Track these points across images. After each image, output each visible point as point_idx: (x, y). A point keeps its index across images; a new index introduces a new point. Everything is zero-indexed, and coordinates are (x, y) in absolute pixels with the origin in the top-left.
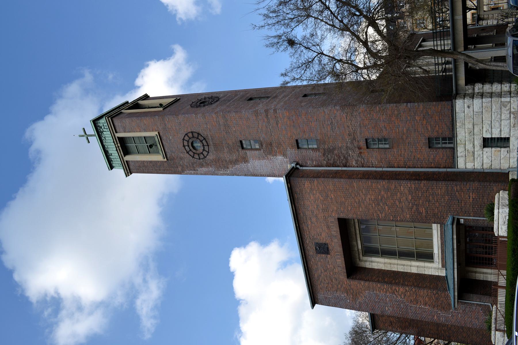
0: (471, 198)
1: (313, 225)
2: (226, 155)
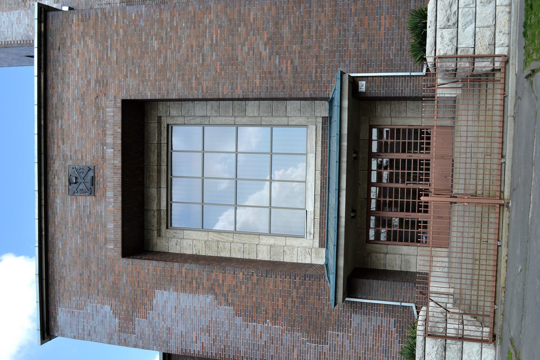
0: (382, 28)
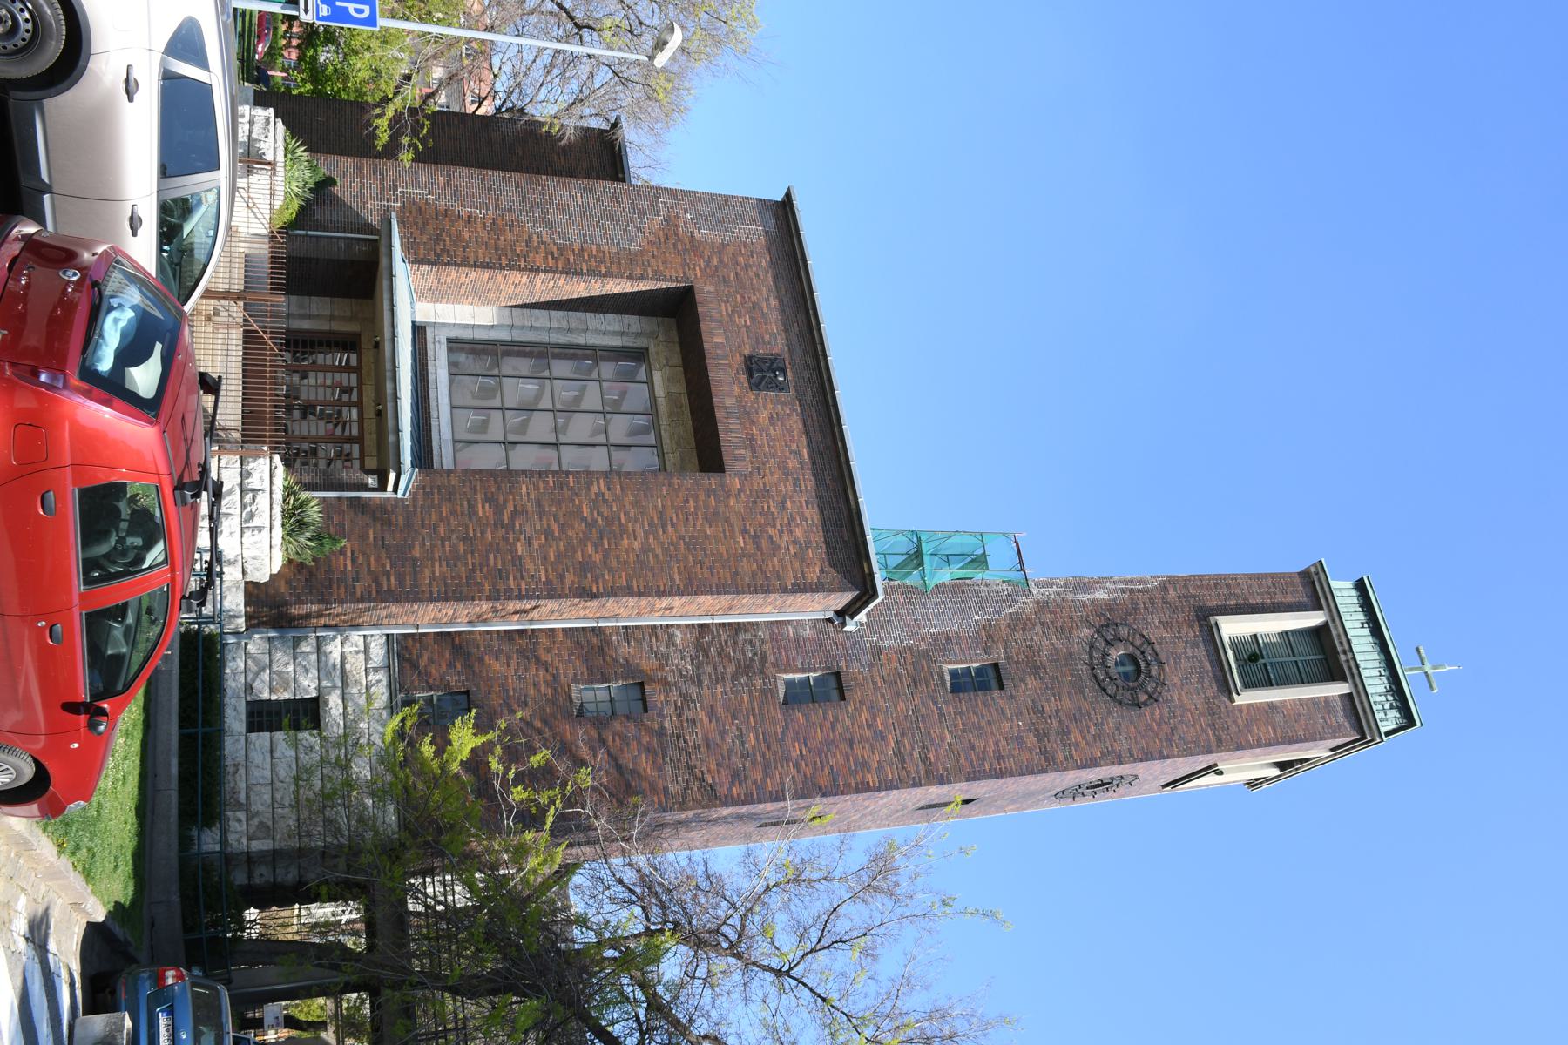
1: (794, 447)
2: (1045, 642)
